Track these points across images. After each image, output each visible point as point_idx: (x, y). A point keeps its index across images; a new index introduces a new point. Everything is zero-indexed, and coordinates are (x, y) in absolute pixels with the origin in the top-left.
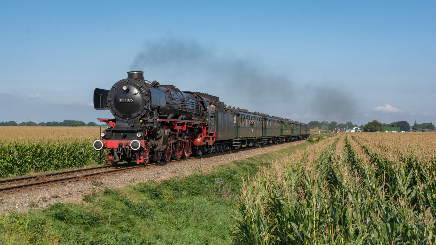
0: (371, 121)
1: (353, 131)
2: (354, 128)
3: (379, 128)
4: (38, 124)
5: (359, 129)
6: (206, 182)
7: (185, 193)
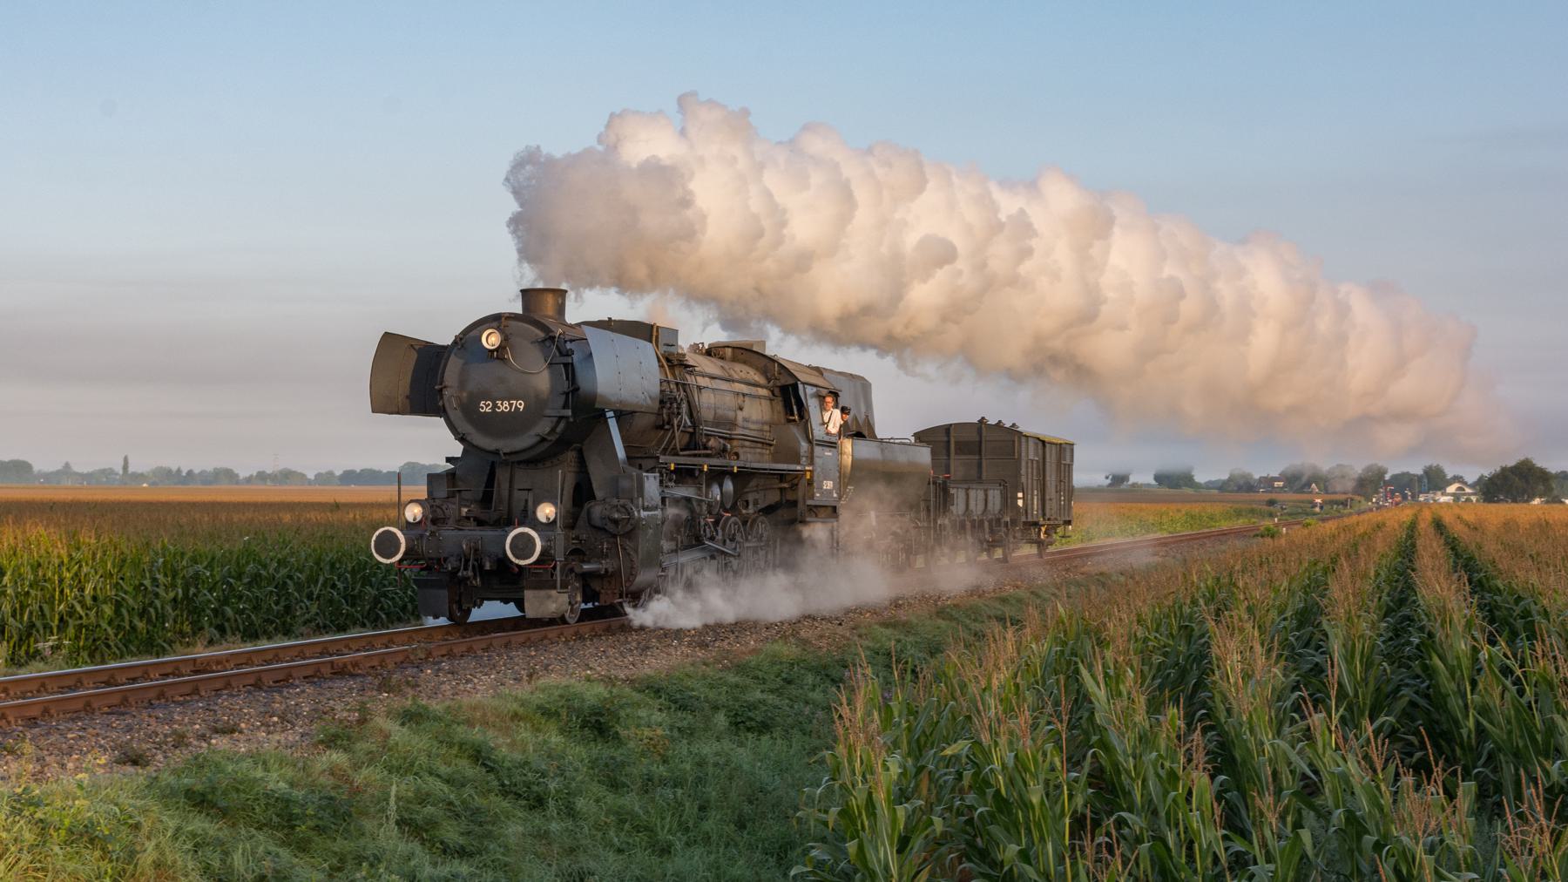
0: (1511, 463)
1: (1443, 499)
2: (1452, 489)
3: (1541, 487)
4: (311, 476)
5: (1468, 490)
6: (810, 679)
7: (721, 720)
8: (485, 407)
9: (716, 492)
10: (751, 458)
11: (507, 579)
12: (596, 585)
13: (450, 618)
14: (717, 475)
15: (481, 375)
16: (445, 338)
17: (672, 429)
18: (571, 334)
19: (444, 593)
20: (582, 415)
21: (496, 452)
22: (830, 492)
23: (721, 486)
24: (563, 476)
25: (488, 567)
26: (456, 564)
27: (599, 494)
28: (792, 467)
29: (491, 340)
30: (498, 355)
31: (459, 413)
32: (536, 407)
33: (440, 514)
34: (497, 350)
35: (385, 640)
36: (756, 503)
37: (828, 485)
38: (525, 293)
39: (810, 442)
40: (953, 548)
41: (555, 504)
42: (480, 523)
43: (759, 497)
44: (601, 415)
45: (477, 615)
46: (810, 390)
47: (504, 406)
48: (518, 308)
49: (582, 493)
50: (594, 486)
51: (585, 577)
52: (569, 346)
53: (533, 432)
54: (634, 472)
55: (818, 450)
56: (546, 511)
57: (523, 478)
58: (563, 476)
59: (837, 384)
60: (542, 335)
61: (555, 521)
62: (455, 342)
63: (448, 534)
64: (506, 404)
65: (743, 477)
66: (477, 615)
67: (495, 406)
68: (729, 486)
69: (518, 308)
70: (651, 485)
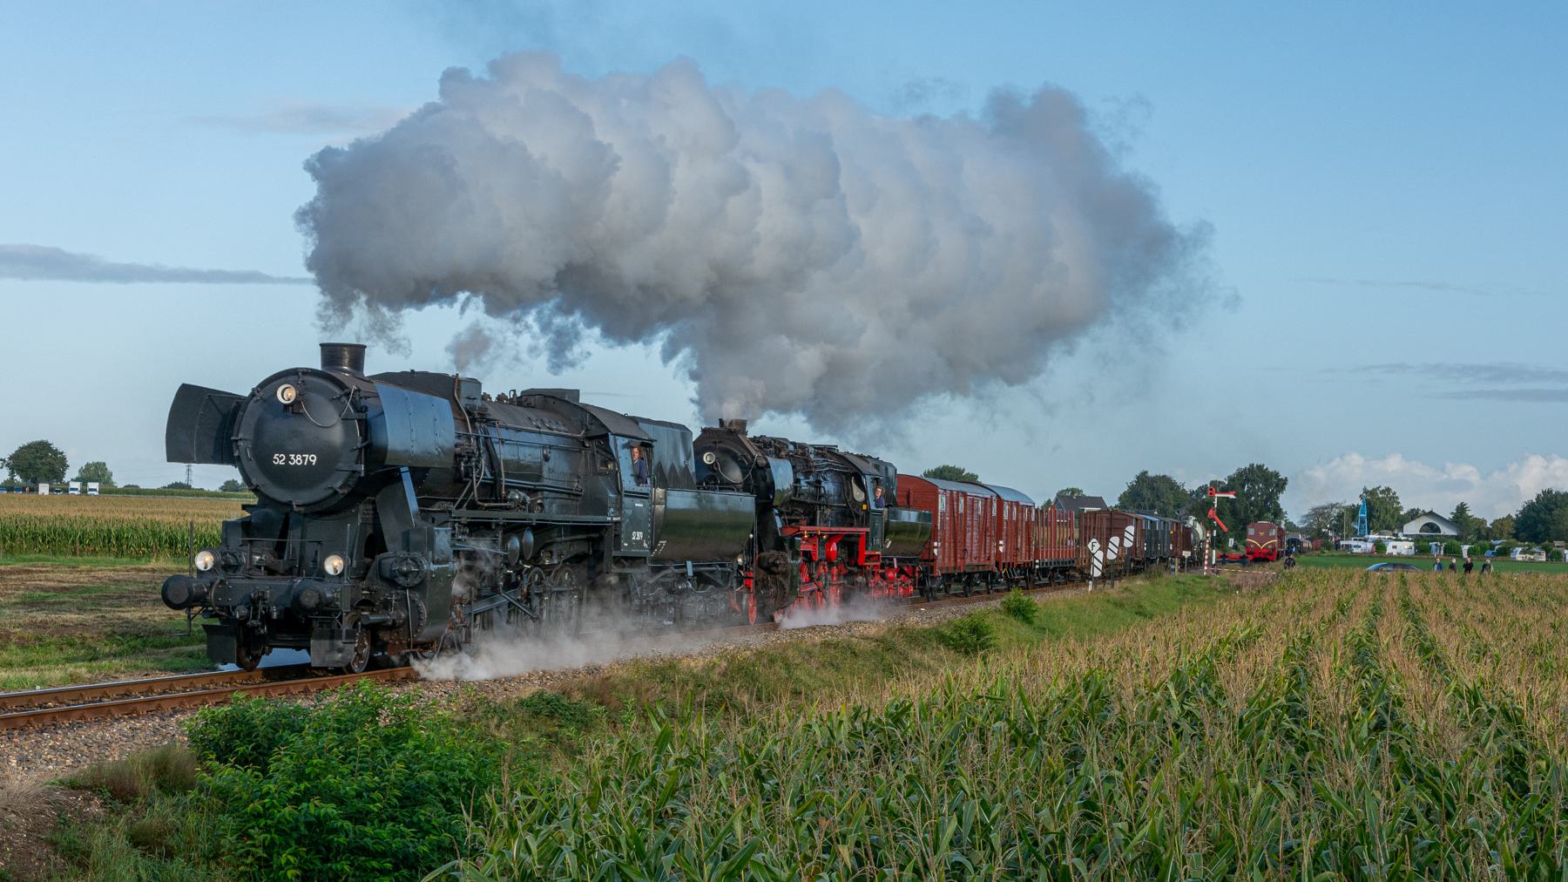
2: (1413, 528)
8: (279, 460)
9: (515, 543)
10: (553, 511)
11: (297, 624)
12: (385, 636)
13: (239, 665)
14: (513, 529)
15: (277, 427)
16: (243, 389)
17: (465, 485)
18: (364, 387)
19: (234, 643)
20: (377, 473)
21: (289, 504)
22: (640, 542)
23: (520, 539)
24: (353, 528)
25: (275, 616)
26: (244, 612)
27: (389, 545)
28: (600, 518)
29: (286, 394)
30: (292, 409)
31: (254, 463)
32: (329, 458)
33: (232, 561)
34: (292, 405)
35: (166, 686)
36: (560, 556)
37: (638, 535)
38: (325, 347)
39: (619, 493)
40: (133, 762)
41: (342, 556)
42: (271, 572)
43: (564, 547)
44: (393, 477)
45: (266, 661)
46: (621, 441)
47: (297, 460)
48: (317, 365)
49: (374, 544)
50: (386, 538)
51: (373, 630)
52: (363, 402)
53: (325, 485)
54: (426, 526)
55: (626, 500)
56: (333, 564)
57: (319, 529)
58: (353, 528)
59: (649, 432)
60: (338, 392)
61: (342, 574)
62: (253, 395)
63: (238, 581)
64: (299, 457)
65: (541, 529)
66: (266, 661)
67: (288, 459)
68: (530, 537)
69: (317, 365)
70: (443, 538)
